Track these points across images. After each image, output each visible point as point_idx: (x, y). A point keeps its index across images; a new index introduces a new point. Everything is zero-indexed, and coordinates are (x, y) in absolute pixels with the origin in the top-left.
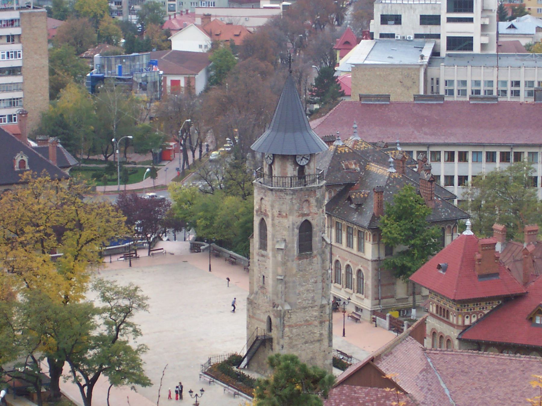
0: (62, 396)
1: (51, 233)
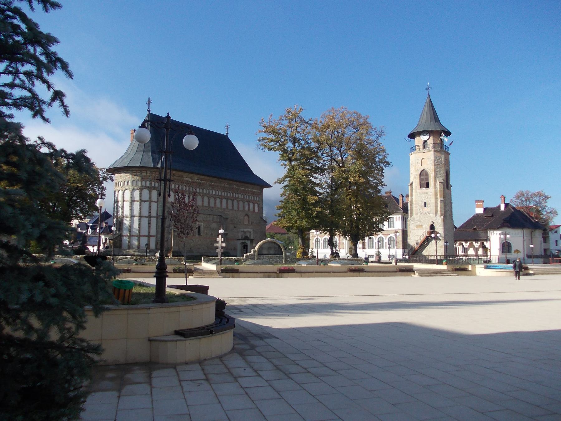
0: (307, 241)
1: (520, 251)
